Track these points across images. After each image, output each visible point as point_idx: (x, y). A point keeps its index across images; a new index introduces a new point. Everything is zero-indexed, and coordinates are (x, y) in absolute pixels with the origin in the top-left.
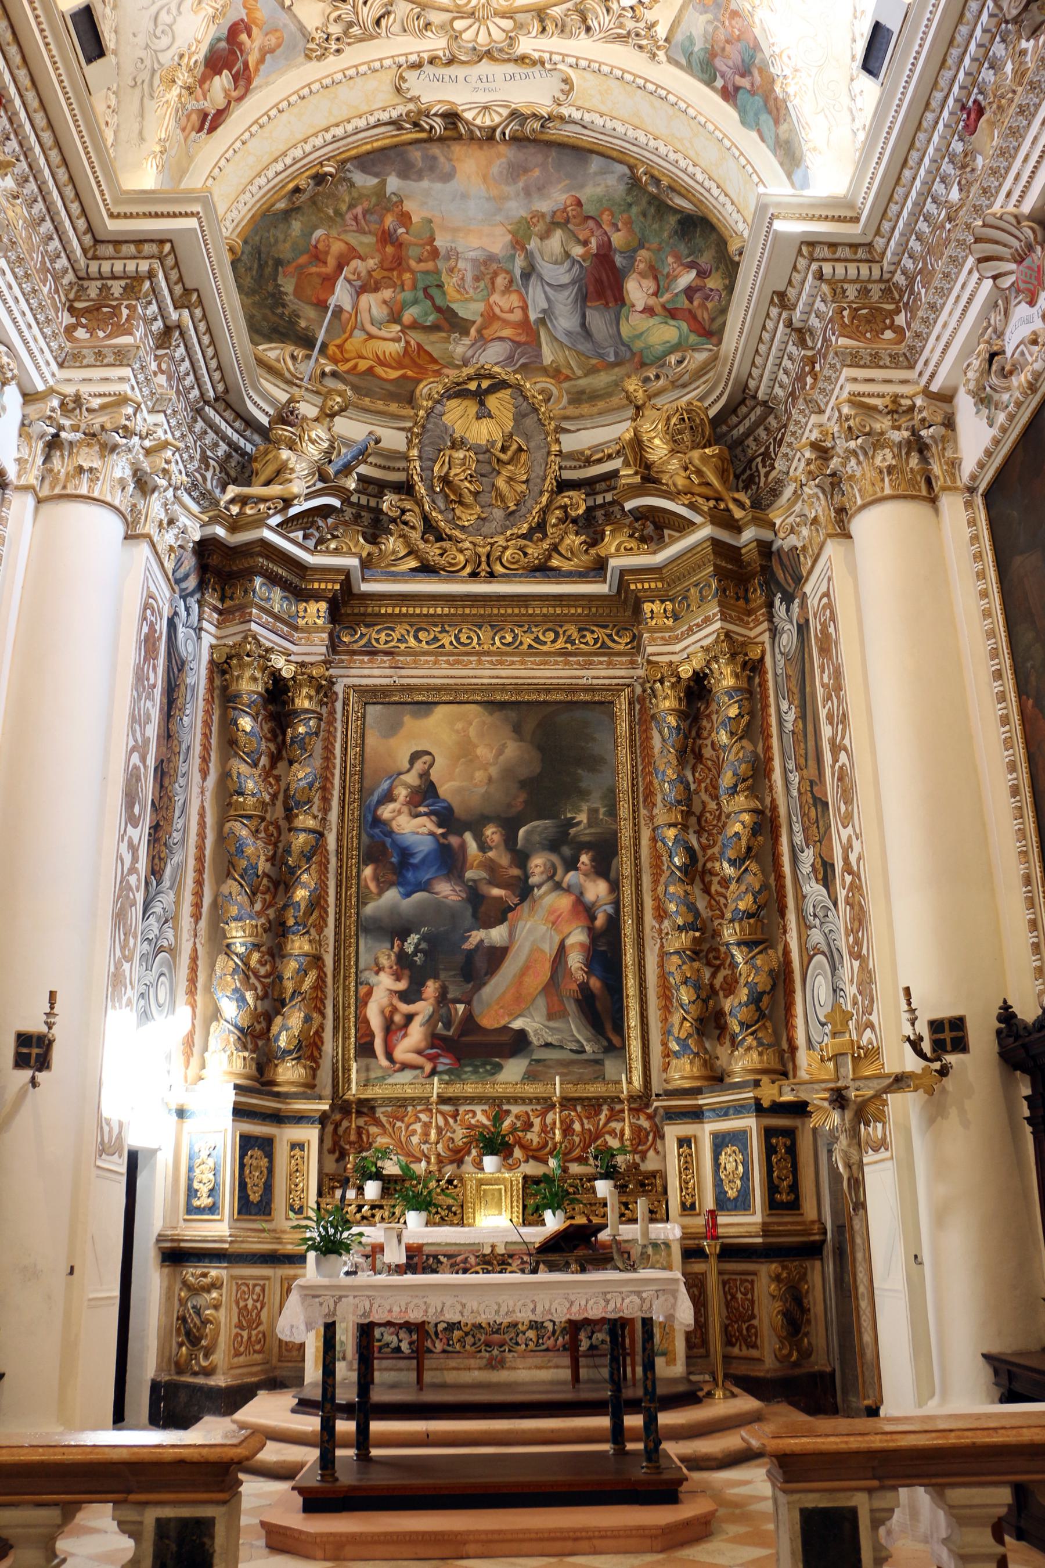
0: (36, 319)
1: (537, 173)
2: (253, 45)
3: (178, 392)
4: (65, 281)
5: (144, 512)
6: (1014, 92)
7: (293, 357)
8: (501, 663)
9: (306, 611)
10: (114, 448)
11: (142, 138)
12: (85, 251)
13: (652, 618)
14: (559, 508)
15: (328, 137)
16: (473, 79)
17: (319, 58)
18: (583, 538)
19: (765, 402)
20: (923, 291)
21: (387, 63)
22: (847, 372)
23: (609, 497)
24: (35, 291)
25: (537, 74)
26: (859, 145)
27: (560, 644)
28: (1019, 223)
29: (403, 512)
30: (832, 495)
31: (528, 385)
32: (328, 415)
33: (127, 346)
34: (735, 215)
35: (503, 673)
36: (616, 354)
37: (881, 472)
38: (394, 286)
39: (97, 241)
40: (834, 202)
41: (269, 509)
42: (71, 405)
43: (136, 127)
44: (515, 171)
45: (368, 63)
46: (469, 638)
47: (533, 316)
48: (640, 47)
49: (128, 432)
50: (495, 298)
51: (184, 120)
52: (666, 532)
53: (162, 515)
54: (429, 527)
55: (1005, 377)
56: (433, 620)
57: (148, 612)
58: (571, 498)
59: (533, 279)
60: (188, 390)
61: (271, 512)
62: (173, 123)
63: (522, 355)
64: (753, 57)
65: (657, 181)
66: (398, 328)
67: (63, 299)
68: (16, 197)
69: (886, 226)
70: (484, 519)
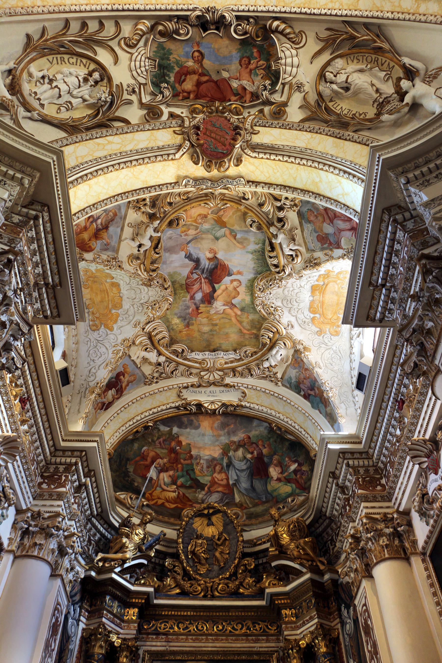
0: (27, 480)
1: (232, 426)
2: (125, 380)
3: (81, 512)
4: (41, 465)
5: (61, 564)
6: (415, 396)
7: (131, 498)
8: (217, 640)
9: (128, 612)
10: (51, 535)
11: (79, 411)
12: (51, 453)
13: (286, 617)
14: (243, 565)
15: (151, 412)
16: (208, 392)
17: (149, 385)
18: (253, 579)
19: (330, 518)
20: (391, 470)
21: (175, 386)
22: (363, 504)
23: (265, 560)
24: (28, 468)
25: (232, 390)
26: (358, 414)
27: (244, 630)
28: (425, 443)
29: (175, 566)
30: (363, 559)
31: (229, 512)
32: (143, 524)
33: (64, 492)
34: (312, 441)
35: (218, 645)
36: (266, 498)
37: (383, 547)
38: (174, 470)
39: (56, 450)
40: (350, 436)
41: (116, 564)
42: (36, 516)
43: (77, 408)
44: (223, 426)
45: (168, 386)
46: (202, 627)
47: (231, 482)
48: (272, 381)
49: (58, 529)
50: (216, 475)
51: (96, 405)
52: (291, 576)
53: (68, 566)
54: (186, 574)
55: (430, 504)
56: (186, 618)
57: (56, 612)
58: (248, 561)
59: (231, 467)
60: (86, 511)
61: (116, 566)
62: (91, 407)
63: (226, 498)
64: (314, 384)
65: (280, 429)
66: (175, 487)
67: (39, 472)
68: (27, 433)
69: (373, 445)
70: (210, 571)
